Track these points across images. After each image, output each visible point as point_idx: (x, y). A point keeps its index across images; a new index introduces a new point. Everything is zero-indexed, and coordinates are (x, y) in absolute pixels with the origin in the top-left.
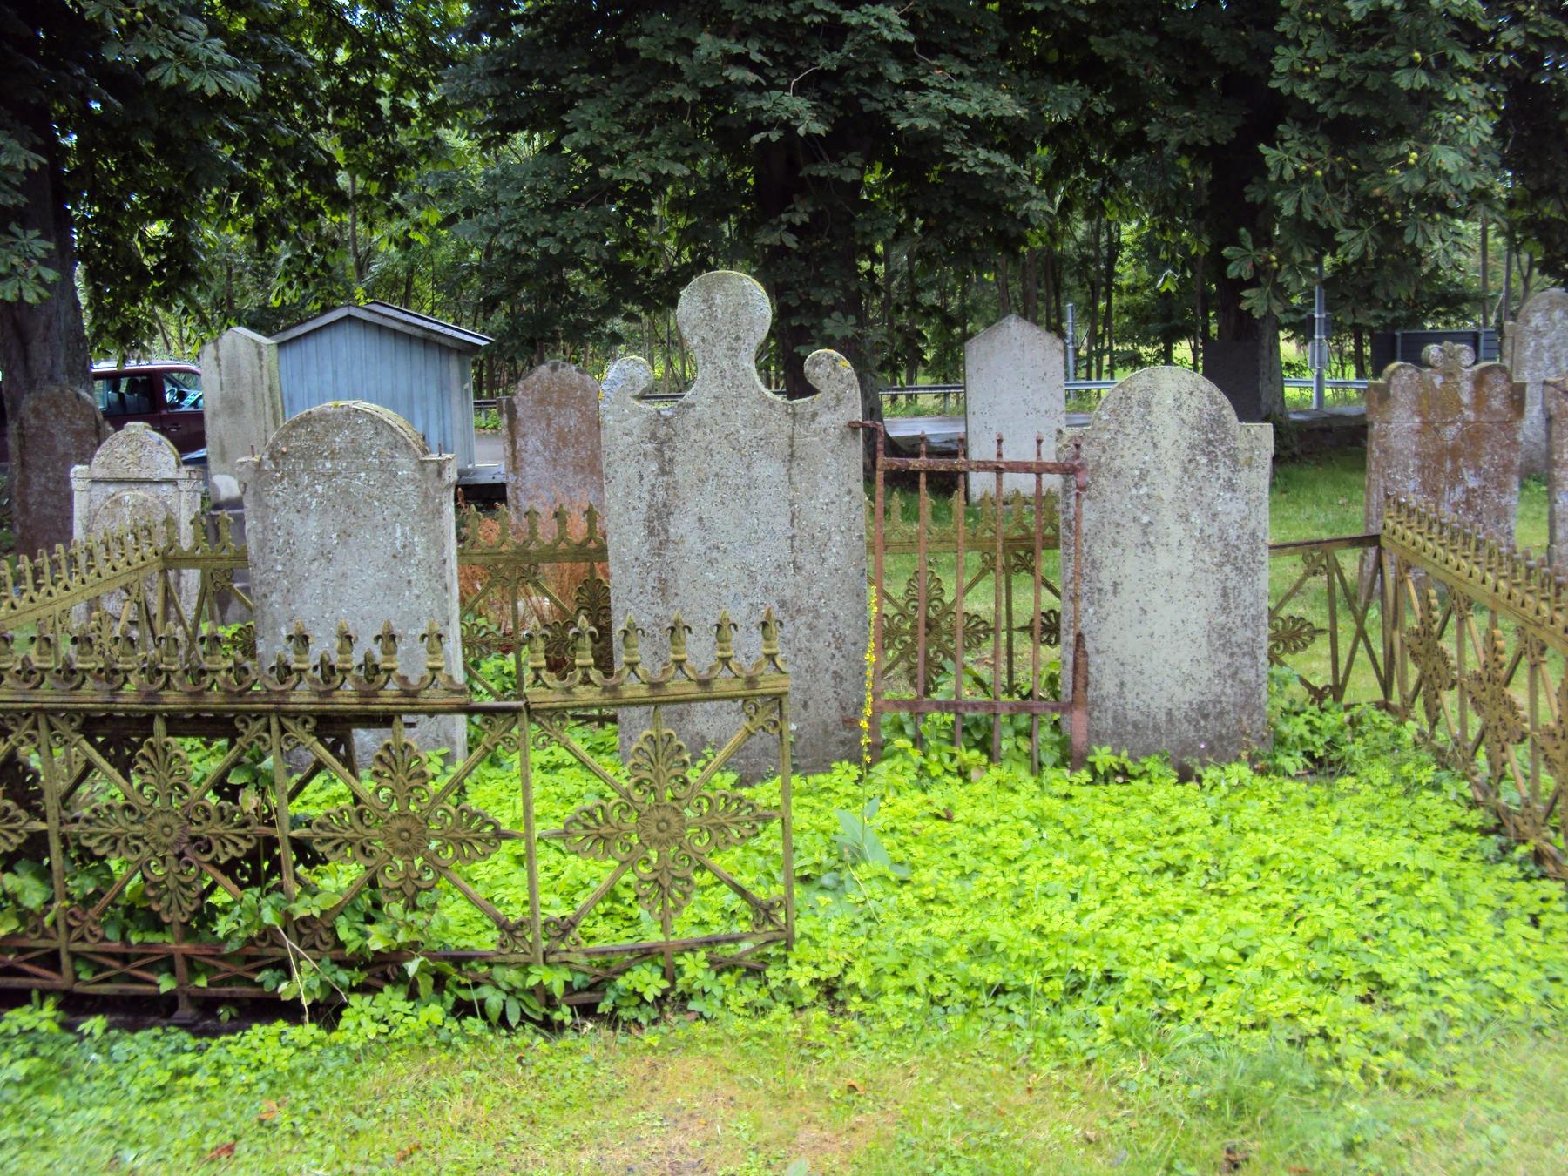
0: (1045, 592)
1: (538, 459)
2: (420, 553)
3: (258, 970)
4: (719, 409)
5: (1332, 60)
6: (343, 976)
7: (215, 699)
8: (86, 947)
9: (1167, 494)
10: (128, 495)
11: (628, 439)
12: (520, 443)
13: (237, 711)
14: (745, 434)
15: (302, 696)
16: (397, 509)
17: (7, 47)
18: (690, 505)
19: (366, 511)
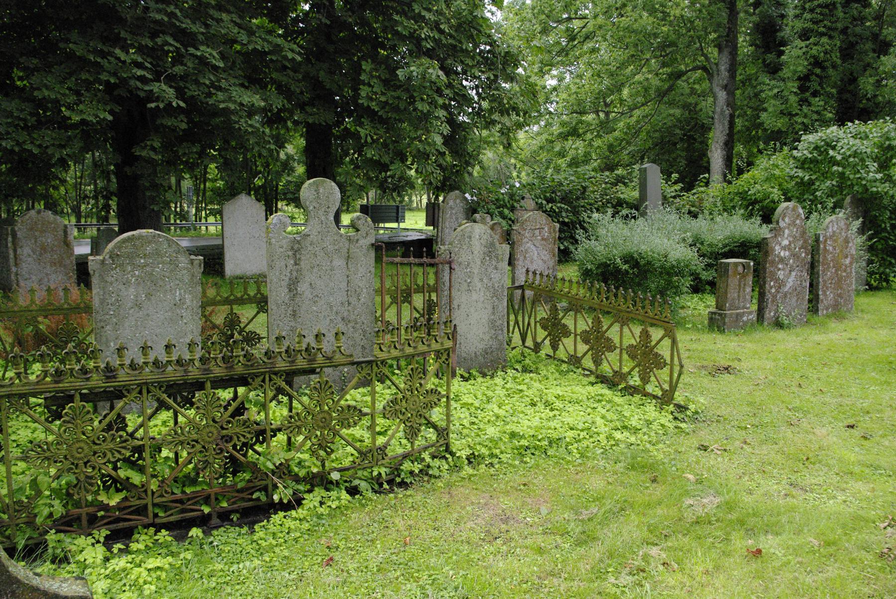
0: (415, 312)
1: (30, 259)
2: (188, 302)
3: (252, 494)
4: (320, 237)
5: (383, 94)
6: (301, 487)
7: (239, 369)
8: (164, 499)
9: (476, 271)
11: (282, 250)
12: (19, 251)
13: (249, 374)
14: (330, 248)
15: (281, 364)
16: (178, 282)
18: (307, 278)
19: (161, 283)
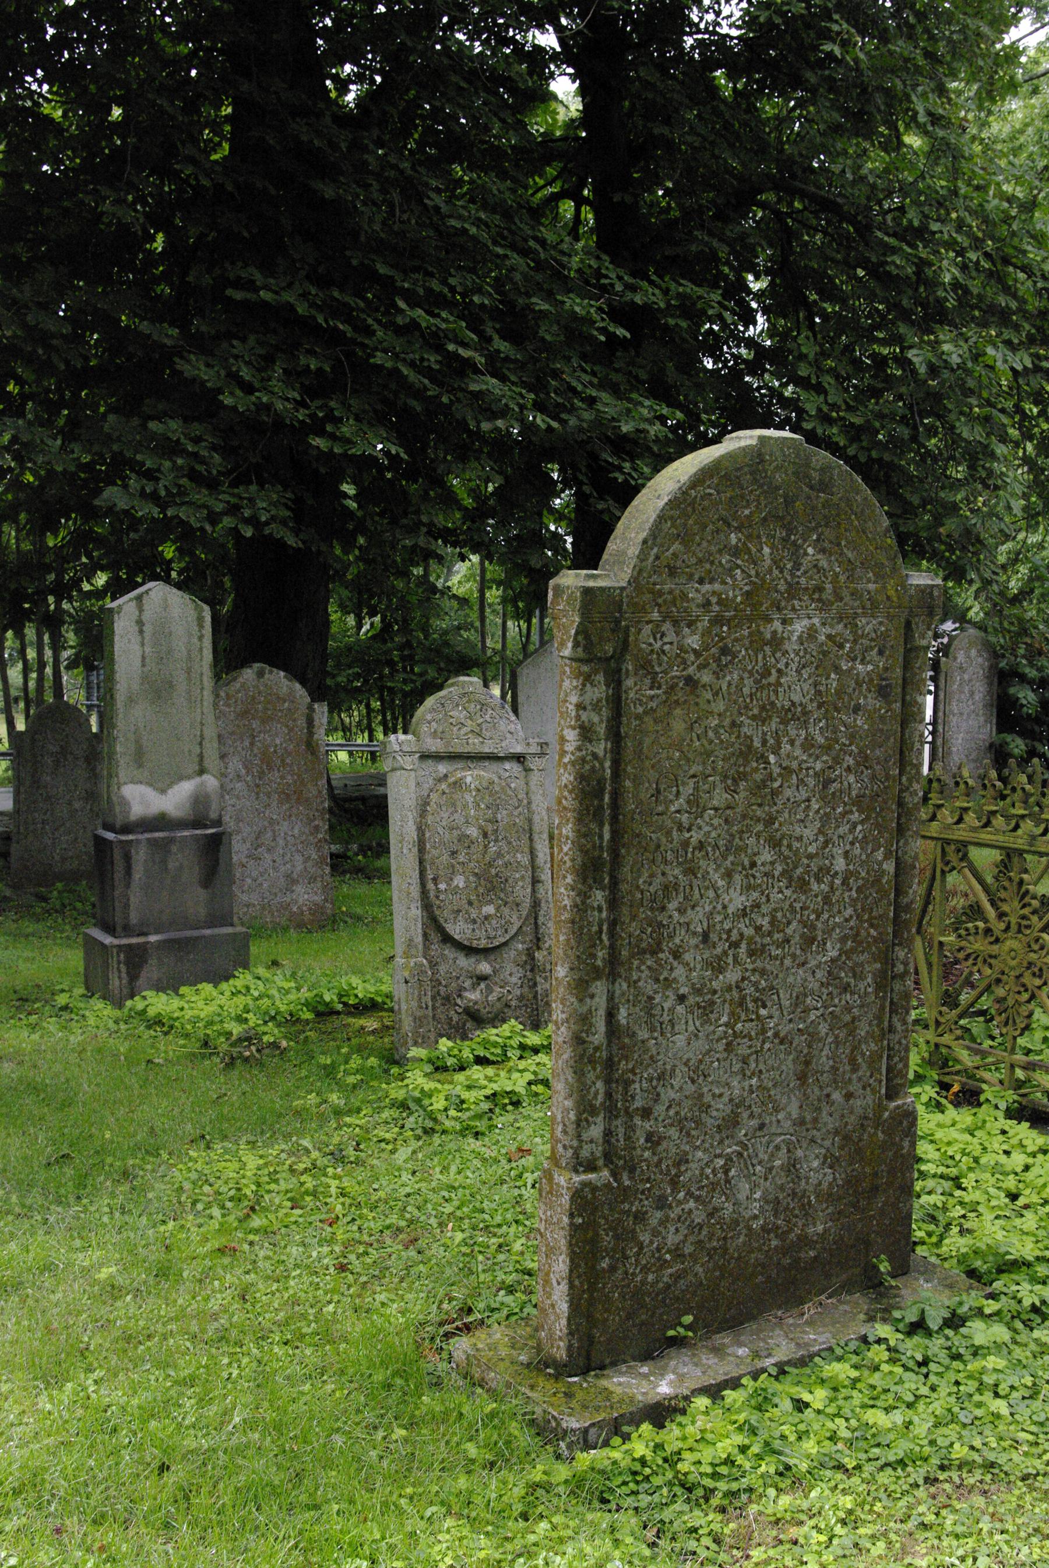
10: (471, 776)
17: (328, 82)
